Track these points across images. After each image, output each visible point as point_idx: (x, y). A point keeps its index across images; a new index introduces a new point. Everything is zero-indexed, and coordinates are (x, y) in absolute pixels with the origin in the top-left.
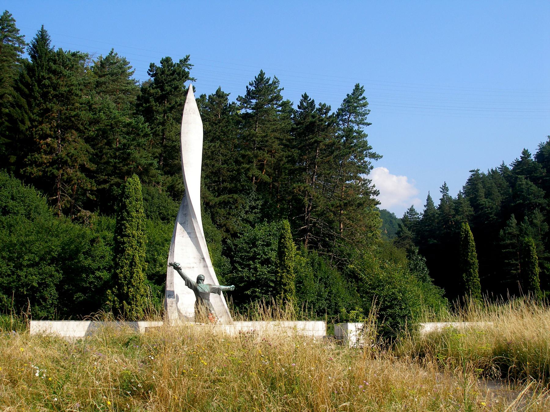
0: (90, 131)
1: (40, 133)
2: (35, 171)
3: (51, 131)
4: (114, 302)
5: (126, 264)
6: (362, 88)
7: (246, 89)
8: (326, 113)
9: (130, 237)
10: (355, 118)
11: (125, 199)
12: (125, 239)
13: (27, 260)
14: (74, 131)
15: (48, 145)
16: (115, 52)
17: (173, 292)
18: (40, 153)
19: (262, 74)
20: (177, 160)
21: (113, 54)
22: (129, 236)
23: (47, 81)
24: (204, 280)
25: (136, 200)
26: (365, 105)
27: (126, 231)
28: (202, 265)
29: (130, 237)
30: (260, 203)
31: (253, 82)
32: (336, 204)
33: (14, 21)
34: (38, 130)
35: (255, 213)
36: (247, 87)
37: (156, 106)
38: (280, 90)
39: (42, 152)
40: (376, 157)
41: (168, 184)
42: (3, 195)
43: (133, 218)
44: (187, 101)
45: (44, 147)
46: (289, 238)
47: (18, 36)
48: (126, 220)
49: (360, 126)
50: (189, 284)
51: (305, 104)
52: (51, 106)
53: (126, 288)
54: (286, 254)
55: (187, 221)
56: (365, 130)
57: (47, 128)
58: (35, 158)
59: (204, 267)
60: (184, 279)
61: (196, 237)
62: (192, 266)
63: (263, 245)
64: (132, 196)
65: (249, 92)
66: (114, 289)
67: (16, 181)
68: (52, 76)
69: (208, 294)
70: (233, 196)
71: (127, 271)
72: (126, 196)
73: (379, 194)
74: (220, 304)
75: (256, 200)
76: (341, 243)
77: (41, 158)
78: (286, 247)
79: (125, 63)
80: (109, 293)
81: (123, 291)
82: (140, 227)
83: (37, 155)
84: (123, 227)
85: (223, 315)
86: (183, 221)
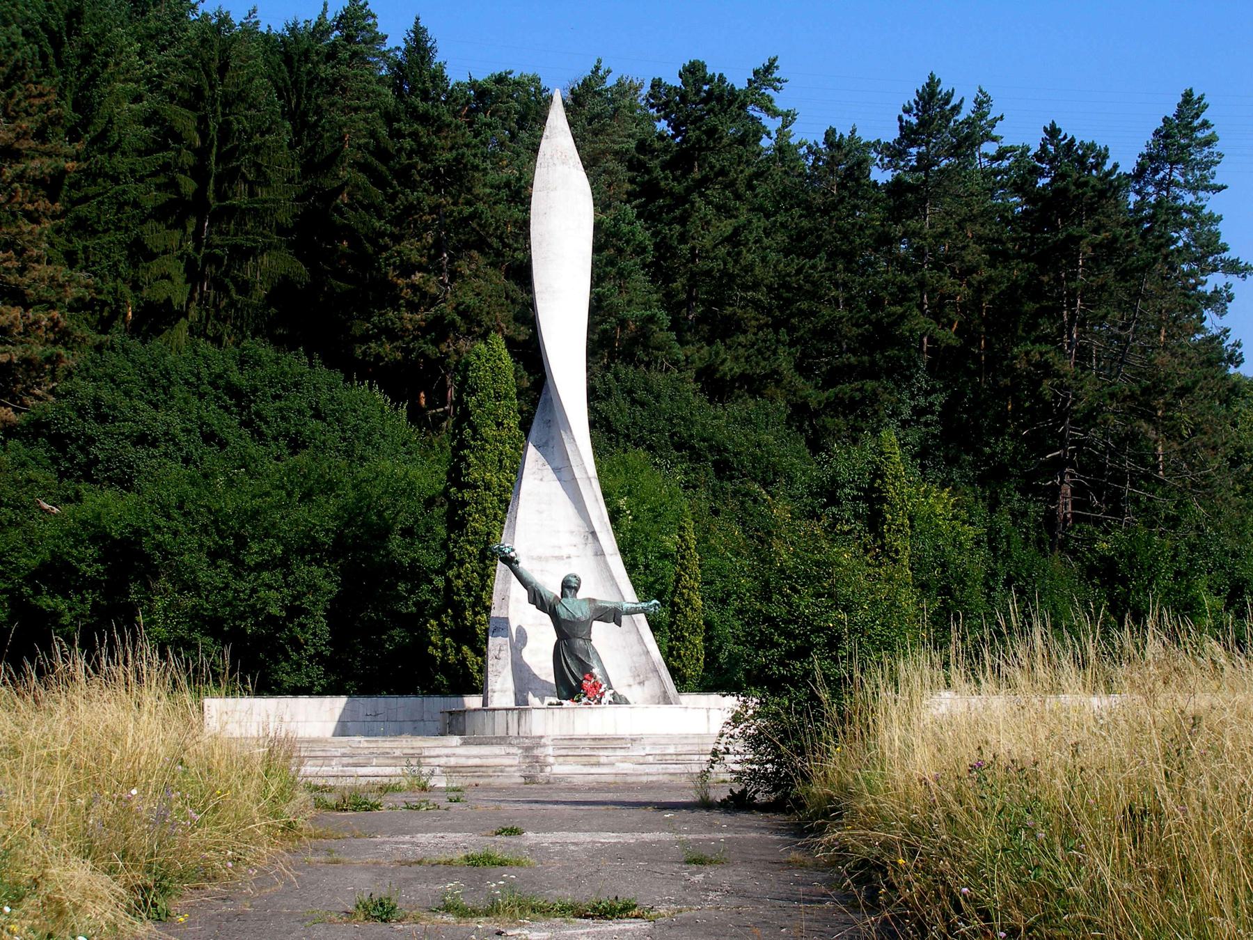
0: (515, 250)
1: (395, 262)
2: (388, 350)
3: (421, 256)
4: (444, 648)
5: (470, 555)
6: (1201, 99)
7: (898, 124)
8: (1097, 166)
9: (479, 487)
10: (1183, 175)
11: (468, 395)
12: (467, 495)
13: (256, 553)
14: (475, 253)
15: (414, 287)
16: (604, 67)
17: (506, 620)
18: (397, 308)
19: (933, 83)
20: (732, 305)
21: (601, 73)
22: (474, 486)
23: (408, 139)
24: (576, 589)
25: (495, 397)
26: (1208, 142)
27: (468, 474)
28: (590, 550)
29: (479, 487)
30: (939, 399)
31: (913, 103)
32: (1122, 392)
33: (374, 16)
34: (392, 256)
35: (927, 425)
36: (900, 119)
37: (666, 178)
38: (995, 120)
39: (401, 305)
40: (1242, 271)
41: (699, 364)
42: (291, 408)
43: (487, 441)
44: (546, 133)
45: (407, 294)
46: (896, 477)
47: (383, 49)
48: (469, 447)
49: (1201, 194)
50: (537, 598)
51: (1051, 148)
52: (418, 198)
53: (468, 614)
54: (886, 519)
55: (553, 438)
56: (1212, 204)
57: (411, 250)
58: (386, 320)
59: (596, 555)
60: (525, 587)
61: (574, 479)
62: (564, 553)
63: (855, 498)
64: (484, 388)
65: (905, 129)
66: (443, 616)
67: (323, 375)
68: (420, 128)
69: (587, 625)
70: (863, 385)
71: (472, 572)
72: (470, 387)
73: (1242, 361)
74: (637, 648)
75: (927, 394)
76: (1153, 492)
77: (401, 319)
78: (884, 500)
79: (535, 80)
80: (432, 626)
81: (463, 622)
82: (507, 463)
83: (391, 314)
84: (463, 465)
85: (647, 678)
86: (544, 441)
